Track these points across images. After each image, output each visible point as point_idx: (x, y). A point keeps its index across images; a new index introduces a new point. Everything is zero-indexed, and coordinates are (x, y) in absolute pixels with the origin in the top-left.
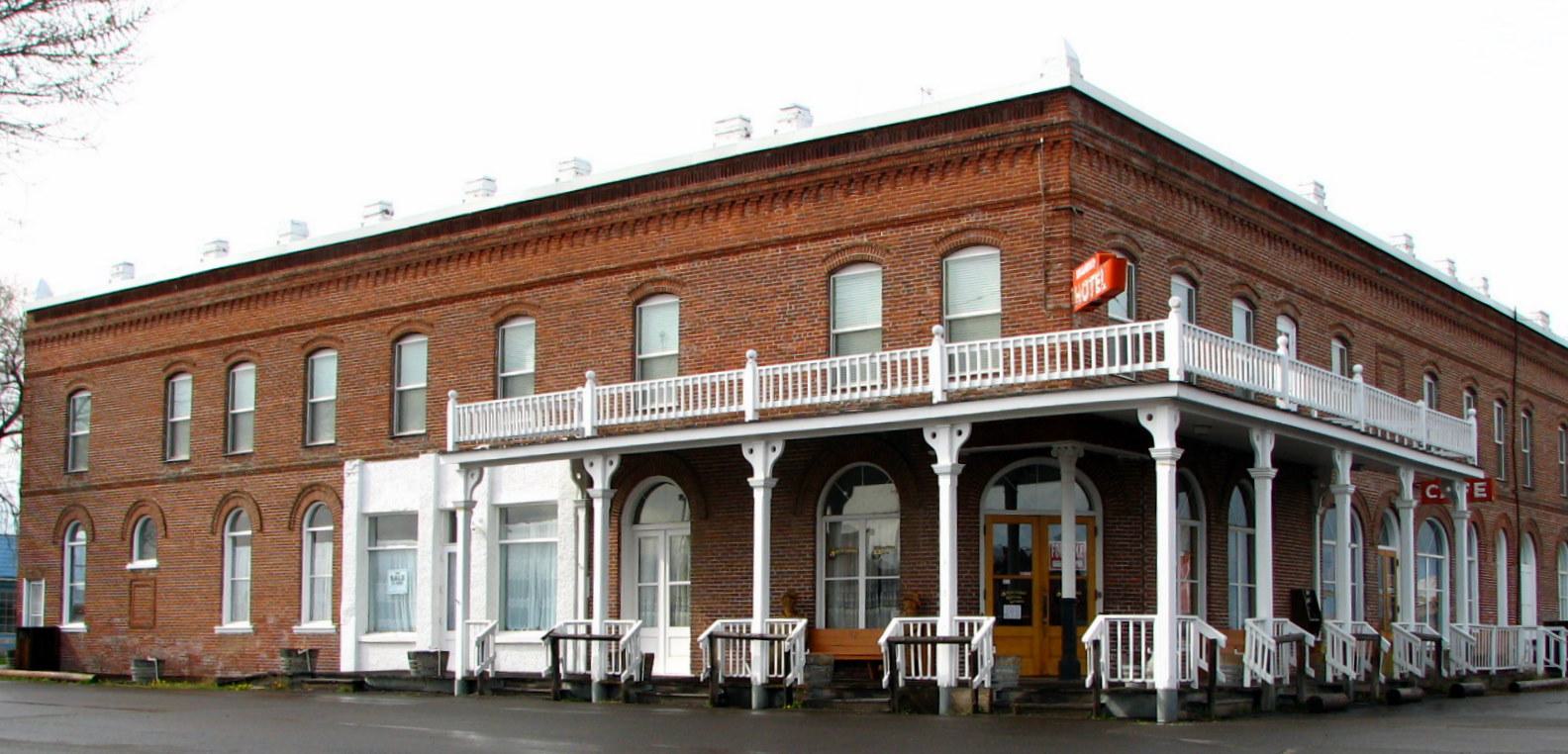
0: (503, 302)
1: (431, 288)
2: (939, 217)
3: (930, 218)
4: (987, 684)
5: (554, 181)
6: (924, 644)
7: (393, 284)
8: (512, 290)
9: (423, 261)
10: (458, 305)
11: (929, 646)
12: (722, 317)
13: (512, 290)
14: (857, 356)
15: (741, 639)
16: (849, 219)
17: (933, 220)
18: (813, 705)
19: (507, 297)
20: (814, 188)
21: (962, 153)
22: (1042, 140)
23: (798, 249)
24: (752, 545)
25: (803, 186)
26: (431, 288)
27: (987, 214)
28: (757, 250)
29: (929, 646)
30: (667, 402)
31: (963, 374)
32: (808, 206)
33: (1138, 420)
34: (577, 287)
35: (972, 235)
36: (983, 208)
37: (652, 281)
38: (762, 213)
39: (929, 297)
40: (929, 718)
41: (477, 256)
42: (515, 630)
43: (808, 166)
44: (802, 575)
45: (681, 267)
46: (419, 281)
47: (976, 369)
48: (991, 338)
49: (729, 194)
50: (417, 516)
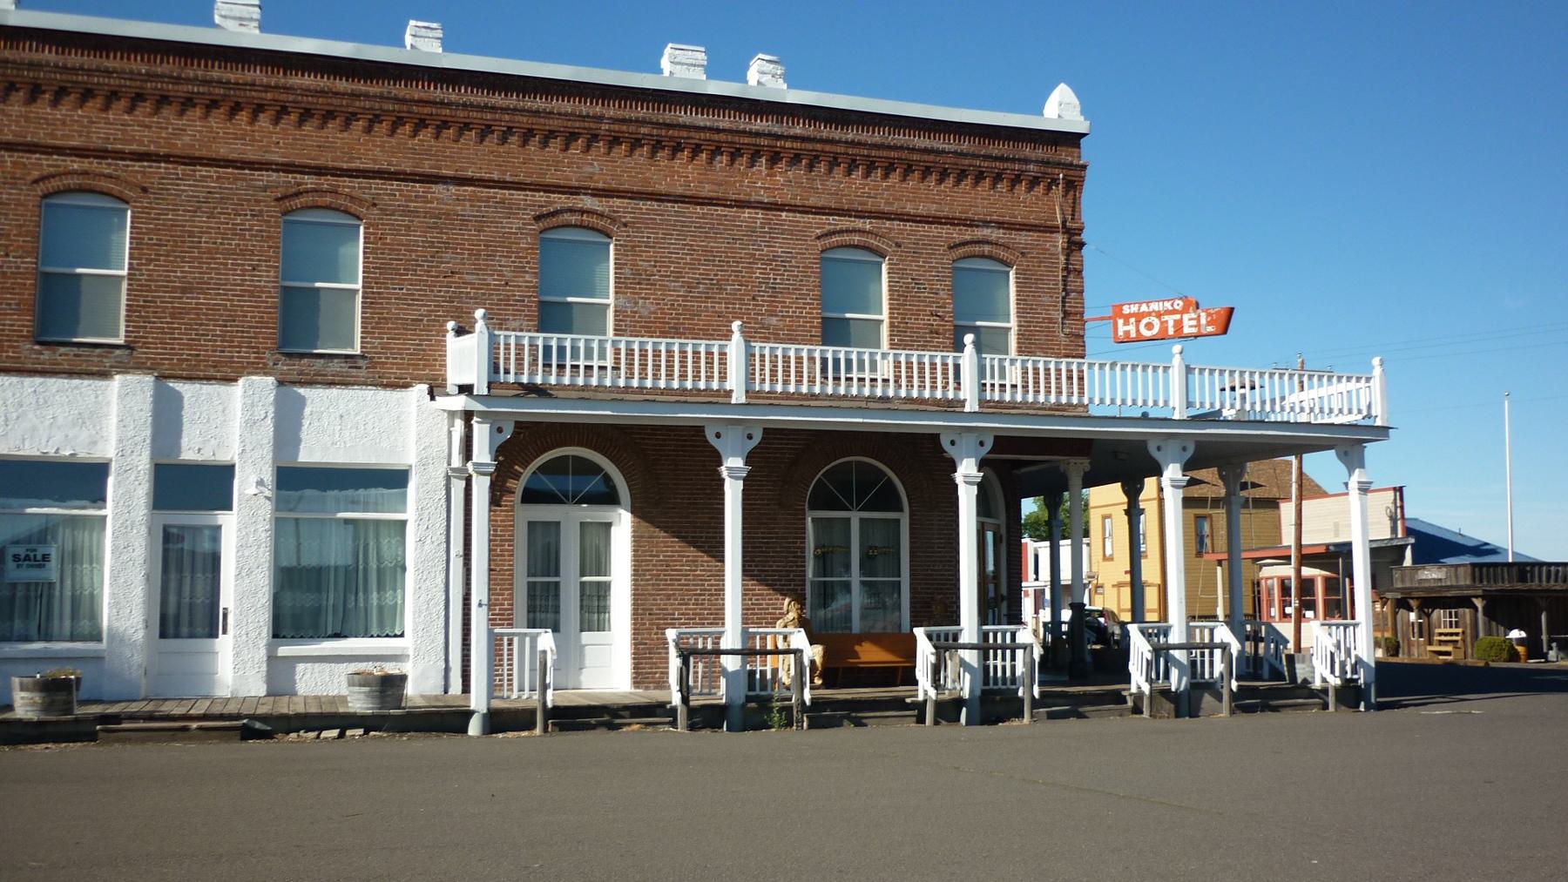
0: (299, 184)
1: (137, 132)
2: (951, 221)
3: (222, 163)
4: (1146, 688)
5: (1056, 117)
6: (1004, 648)
7: (48, 110)
8: (319, 171)
9: (1008, 174)
10: (203, 171)
11: (991, 651)
12: (681, 272)
13: (319, 171)
14: (856, 350)
15: (1004, 648)
16: (182, 144)
17: (945, 224)
18: (822, 715)
19: (309, 181)
20: (808, 156)
21: (980, 166)
22: (1061, 176)
23: (784, 217)
24: (723, 537)
25: (111, 88)
26: (137, 132)
27: (1001, 231)
28: (730, 206)
29: (991, 651)
30: (599, 359)
31: (1002, 382)
32: (798, 172)
33: (1148, 452)
34: (439, 189)
35: (987, 249)
36: (1000, 225)
37: (571, 210)
38: (736, 165)
39: (941, 299)
40: (459, 736)
41: (99, 102)
42: (302, 637)
43: (798, 130)
44: (792, 574)
45: (617, 202)
46: (111, 116)
47: (592, 359)
48: (870, 348)
49: (655, 132)
50: (233, 466)
